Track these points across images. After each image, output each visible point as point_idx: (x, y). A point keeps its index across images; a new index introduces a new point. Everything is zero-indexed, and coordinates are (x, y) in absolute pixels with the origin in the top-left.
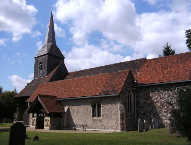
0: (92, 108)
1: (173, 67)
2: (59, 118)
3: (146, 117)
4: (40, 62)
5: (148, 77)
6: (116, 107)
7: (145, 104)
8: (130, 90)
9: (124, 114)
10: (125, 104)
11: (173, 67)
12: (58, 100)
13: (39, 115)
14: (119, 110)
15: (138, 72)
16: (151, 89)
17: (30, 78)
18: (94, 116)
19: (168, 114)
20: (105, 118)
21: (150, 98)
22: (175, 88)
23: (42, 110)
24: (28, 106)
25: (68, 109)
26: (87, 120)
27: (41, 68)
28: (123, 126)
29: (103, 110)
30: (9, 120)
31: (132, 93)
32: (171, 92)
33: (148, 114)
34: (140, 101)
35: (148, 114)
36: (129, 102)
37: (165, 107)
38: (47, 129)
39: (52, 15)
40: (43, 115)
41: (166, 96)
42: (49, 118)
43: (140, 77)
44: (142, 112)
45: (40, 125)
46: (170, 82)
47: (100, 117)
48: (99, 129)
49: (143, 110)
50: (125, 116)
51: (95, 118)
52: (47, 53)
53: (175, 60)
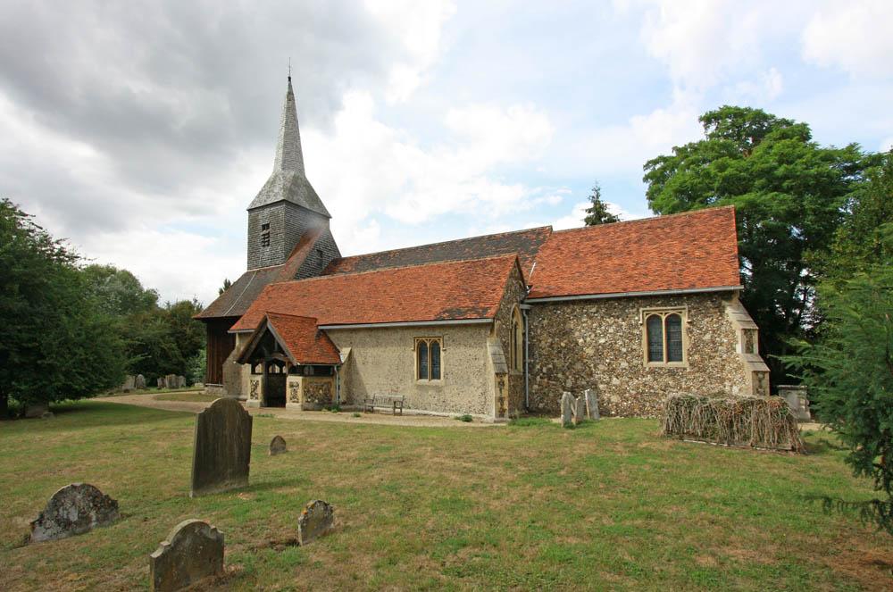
0: (415, 354)
1: (629, 253)
2: (326, 380)
3: (554, 382)
4: (262, 223)
5: (562, 278)
6: (482, 354)
7: (553, 348)
8: (514, 309)
9: (504, 374)
10: (505, 346)
11: (629, 253)
12: (322, 330)
13: (270, 369)
14: (491, 362)
15: (531, 262)
16: (569, 311)
17: (236, 266)
18: (421, 375)
19: (615, 379)
20: (451, 381)
21: (566, 333)
22: (635, 310)
23: (280, 357)
24: (237, 344)
25: (351, 354)
26: (401, 387)
27: (266, 241)
28: (502, 405)
29: (447, 362)
30: (182, 380)
31: (518, 319)
32: (624, 320)
33: (560, 375)
34: (540, 341)
35: (560, 375)
36: (513, 341)
37: (607, 361)
38: (294, 407)
39: (290, 86)
40: (281, 370)
41: (611, 330)
42: (301, 378)
43: (541, 275)
44: (544, 370)
45: (274, 397)
46: (625, 294)
47: (439, 378)
48: (436, 410)
49: (546, 365)
50: (506, 379)
51: (424, 381)
52: (280, 198)
53: (634, 235)
